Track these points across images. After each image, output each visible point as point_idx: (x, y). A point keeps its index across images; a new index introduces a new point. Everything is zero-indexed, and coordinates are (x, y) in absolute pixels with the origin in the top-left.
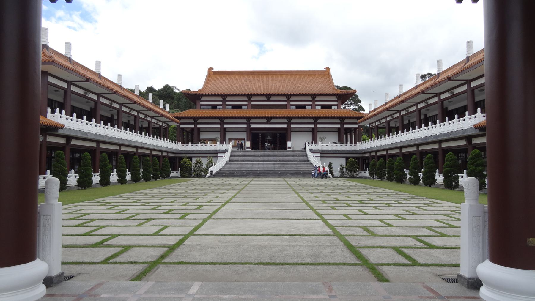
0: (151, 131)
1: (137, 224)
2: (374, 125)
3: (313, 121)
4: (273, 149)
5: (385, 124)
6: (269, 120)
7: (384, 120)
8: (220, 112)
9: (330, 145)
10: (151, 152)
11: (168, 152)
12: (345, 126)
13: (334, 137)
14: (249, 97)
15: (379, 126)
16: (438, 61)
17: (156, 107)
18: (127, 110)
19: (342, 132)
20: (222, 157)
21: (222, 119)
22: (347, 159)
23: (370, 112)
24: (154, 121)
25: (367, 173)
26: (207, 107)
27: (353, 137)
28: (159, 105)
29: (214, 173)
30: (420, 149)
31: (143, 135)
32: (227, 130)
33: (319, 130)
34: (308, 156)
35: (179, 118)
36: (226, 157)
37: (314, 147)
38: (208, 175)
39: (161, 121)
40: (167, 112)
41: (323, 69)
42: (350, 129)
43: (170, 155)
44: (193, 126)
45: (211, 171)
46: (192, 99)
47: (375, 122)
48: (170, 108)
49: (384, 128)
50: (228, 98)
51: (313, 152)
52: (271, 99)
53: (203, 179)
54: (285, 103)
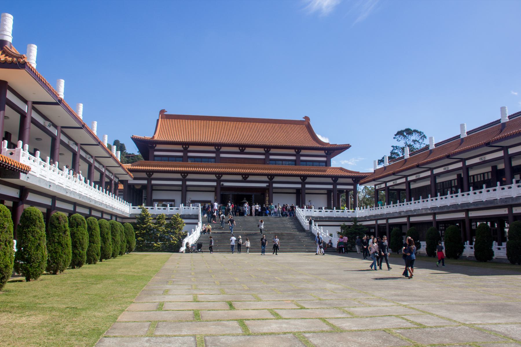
3: (146, 176)
6: (245, 177)
12: (339, 187)
13: (323, 200)
22: (343, 227)
30: (437, 218)
32: (154, 188)
33: (274, 190)
38: (183, 249)
41: (301, 118)
44: (145, 182)
45: (187, 244)
54: (263, 157)
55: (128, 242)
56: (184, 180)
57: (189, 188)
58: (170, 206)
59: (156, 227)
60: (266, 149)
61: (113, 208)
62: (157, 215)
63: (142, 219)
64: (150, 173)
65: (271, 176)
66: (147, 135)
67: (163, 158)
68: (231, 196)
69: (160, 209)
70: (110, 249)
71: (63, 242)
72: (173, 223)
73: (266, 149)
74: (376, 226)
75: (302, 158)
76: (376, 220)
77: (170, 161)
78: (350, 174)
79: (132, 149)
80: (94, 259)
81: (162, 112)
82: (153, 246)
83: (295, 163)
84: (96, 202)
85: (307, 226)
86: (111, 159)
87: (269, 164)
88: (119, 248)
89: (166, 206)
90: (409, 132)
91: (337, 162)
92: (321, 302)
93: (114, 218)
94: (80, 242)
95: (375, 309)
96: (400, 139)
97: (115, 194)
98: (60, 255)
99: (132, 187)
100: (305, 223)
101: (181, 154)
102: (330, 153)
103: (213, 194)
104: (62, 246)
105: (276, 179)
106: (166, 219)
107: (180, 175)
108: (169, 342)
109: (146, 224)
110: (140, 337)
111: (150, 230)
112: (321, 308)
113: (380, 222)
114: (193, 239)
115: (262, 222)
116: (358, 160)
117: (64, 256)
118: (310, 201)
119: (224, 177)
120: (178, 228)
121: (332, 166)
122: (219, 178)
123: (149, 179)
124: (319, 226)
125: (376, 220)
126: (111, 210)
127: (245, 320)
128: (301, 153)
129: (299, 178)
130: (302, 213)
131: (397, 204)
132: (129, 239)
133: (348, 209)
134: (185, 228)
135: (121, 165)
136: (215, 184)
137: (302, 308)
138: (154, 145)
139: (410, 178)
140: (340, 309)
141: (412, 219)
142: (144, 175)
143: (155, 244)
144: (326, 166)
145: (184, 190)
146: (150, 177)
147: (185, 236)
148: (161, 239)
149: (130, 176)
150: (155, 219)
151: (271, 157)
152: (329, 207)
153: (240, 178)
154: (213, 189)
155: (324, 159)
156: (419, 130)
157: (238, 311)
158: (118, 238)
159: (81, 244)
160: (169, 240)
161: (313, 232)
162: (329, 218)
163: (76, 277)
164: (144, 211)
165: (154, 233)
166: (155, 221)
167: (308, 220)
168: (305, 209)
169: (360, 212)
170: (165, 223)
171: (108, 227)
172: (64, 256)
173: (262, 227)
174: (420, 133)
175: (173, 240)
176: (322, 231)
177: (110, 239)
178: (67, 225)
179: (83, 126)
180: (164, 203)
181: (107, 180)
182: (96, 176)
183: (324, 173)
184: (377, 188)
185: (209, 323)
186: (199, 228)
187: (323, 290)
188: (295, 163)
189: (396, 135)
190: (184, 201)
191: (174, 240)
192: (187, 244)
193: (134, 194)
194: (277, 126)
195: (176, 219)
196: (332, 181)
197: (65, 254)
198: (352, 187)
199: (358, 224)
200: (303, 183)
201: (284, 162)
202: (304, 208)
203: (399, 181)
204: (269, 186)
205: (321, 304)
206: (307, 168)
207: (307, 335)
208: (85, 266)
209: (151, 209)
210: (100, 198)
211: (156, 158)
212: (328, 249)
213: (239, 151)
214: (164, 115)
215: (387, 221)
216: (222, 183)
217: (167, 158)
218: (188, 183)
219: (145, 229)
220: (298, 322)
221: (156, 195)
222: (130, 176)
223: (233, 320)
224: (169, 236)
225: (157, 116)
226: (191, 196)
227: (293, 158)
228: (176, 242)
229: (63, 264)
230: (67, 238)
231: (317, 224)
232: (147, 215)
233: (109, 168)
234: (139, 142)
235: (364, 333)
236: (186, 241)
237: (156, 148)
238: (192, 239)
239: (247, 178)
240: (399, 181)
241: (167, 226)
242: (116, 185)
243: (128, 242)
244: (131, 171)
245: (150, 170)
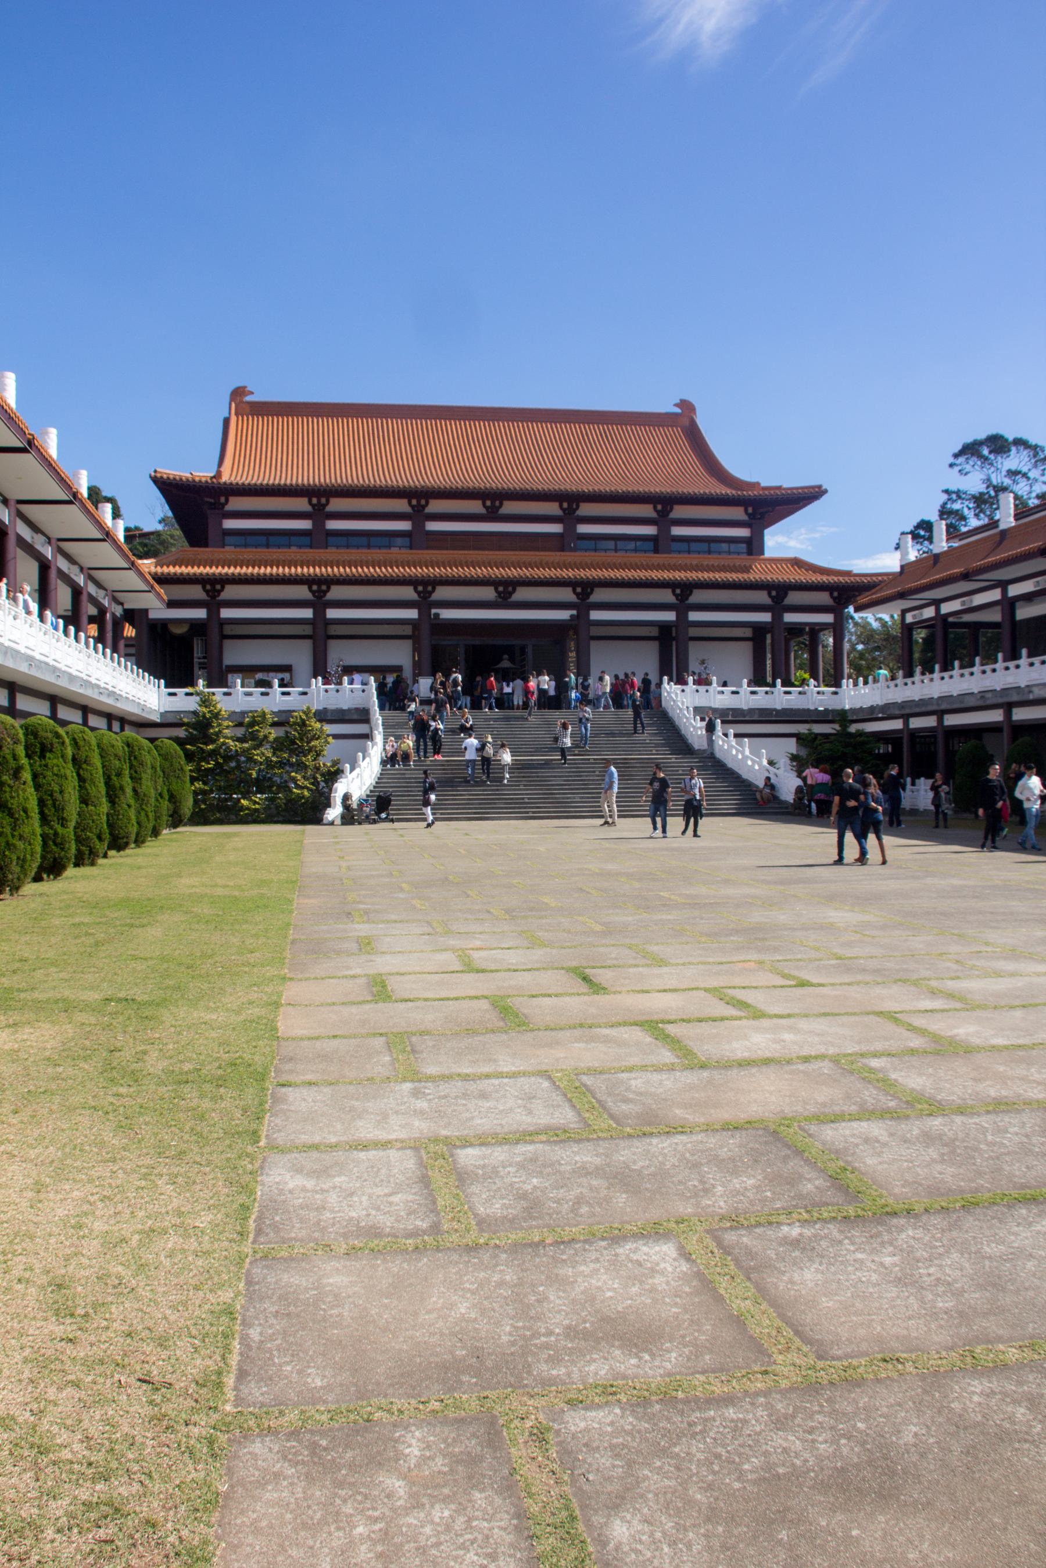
6: (505, 592)
12: (790, 618)
13: (741, 656)
26: (733, 547)
32: (228, 630)
33: (594, 631)
38: (334, 813)
41: (668, 406)
44: (201, 614)
45: (346, 797)
50: (586, 509)
54: (556, 528)
55: (172, 798)
56: (319, 604)
57: (334, 630)
58: (280, 686)
59: (245, 751)
60: (659, 507)
61: (117, 697)
62: (243, 713)
63: (200, 728)
64: (213, 585)
65: (585, 588)
66: (199, 469)
67: (354, 540)
68: (461, 650)
70: (129, 819)
71: (14, 804)
72: (295, 737)
73: (488, 503)
74: (905, 733)
75: (677, 531)
76: (906, 717)
77: (375, 547)
78: (825, 578)
79: (151, 513)
80: (91, 852)
81: (238, 393)
82: (237, 807)
83: (656, 544)
84: (72, 678)
85: (700, 737)
86: (106, 546)
87: (575, 550)
88: (151, 815)
89: (268, 684)
90: (998, 444)
91: (783, 541)
92: (845, 965)
93: (116, 726)
94: (54, 801)
95: (1019, 982)
96: (968, 468)
97: (115, 650)
98: (7, 843)
99: (159, 630)
100: (694, 729)
101: (305, 525)
102: (762, 515)
103: (408, 645)
104: (11, 814)
105: (599, 595)
106: (274, 724)
107: (669, 591)
108: (484, 1096)
109: (213, 741)
110: (382, 1082)
111: (228, 758)
112: (858, 983)
113: (915, 723)
114: (362, 783)
115: (565, 726)
116: (817, 535)
117: (20, 845)
118: (703, 662)
119: (442, 593)
120: (310, 750)
121: (768, 554)
122: (319, 595)
123: (213, 604)
124: (736, 736)
125: (906, 717)
126: (110, 701)
127: (663, 1022)
128: (428, 510)
129: (570, 589)
130: (681, 699)
131: (975, 669)
132: (174, 787)
133: (819, 686)
134: (331, 752)
135: (133, 563)
136: (412, 614)
137: (803, 984)
138: (223, 500)
139: (1014, 590)
140: (916, 983)
141: (1020, 715)
142: (197, 592)
143: (244, 802)
144: (750, 553)
145: (320, 636)
146: (213, 597)
147: (333, 775)
148: (262, 784)
149: (158, 595)
150: (240, 724)
151: (583, 529)
152: (758, 679)
153: (488, 593)
154: (408, 630)
155: (743, 532)
156: (1033, 441)
157: (619, 997)
158: (147, 786)
159: (59, 809)
160: (284, 787)
161: (718, 754)
162: (762, 711)
163: (68, 907)
164: (205, 702)
165: (238, 767)
166: (240, 732)
167: (702, 719)
168: (691, 686)
169: (854, 695)
170: (272, 737)
171: (121, 753)
172: (20, 845)
173: (568, 742)
174: (1035, 449)
175: (298, 787)
176: (747, 752)
177: (129, 791)
178: (21, 751)
179: (30, 443)
180: (259, 676)
181: (93, 611)
182: (63, 596)
183: (746, 576)
184: (909, 618)
185: (560, 1034)
186: (376, 750)
187: (829, 928)
188: (656, 544)
189: (956, 456)
190: (320, 669)
191: (301, 787)
192: (346, 797)
193: (167, 653)
194: (594, 431)
195: (303, 724)
196: (309, 596)
197: (21, 837)
198: (828, 618)
199: (853, 728)
200: (682, 607)
201: (620, 544)
202: (685, 683)
203: (979, 599)
204: (578, 616)
205: (849, 970)
206: (694, 559)
207: (875, 1063)
208: (71, 871)
209: (263, 694)
210: (80, 666)
211: (228, 539)
212: (758, 802)
213: (483, 511)
214: (246, 406)
215: (940, 720)
216: (433, 611)
217: (263, 539)
218: (332, 613)
219: (214, 753)
220: (820, 1025)
221: (235, 654)
222: (158, 595)
223: (625, 1024)
224: (286, 777)
225: (222, 407)
226: (339, 653)
227: (650, 530)
228: (306, 793)
229: (17, 869)
230: (24, 791)
231: (731, 732)
232: (216, 715)
233: (99, 575)
234: (178, 493)
235: (1034, 1053)
236: (340, 788)
237: (229, 507)
238: (357, 782)
239: (511, 594)
240: (979, 599)
241: (279, 745)
242: (118, 625)
243: (172, 798)
244: (162, 580)
245: (211, 575)
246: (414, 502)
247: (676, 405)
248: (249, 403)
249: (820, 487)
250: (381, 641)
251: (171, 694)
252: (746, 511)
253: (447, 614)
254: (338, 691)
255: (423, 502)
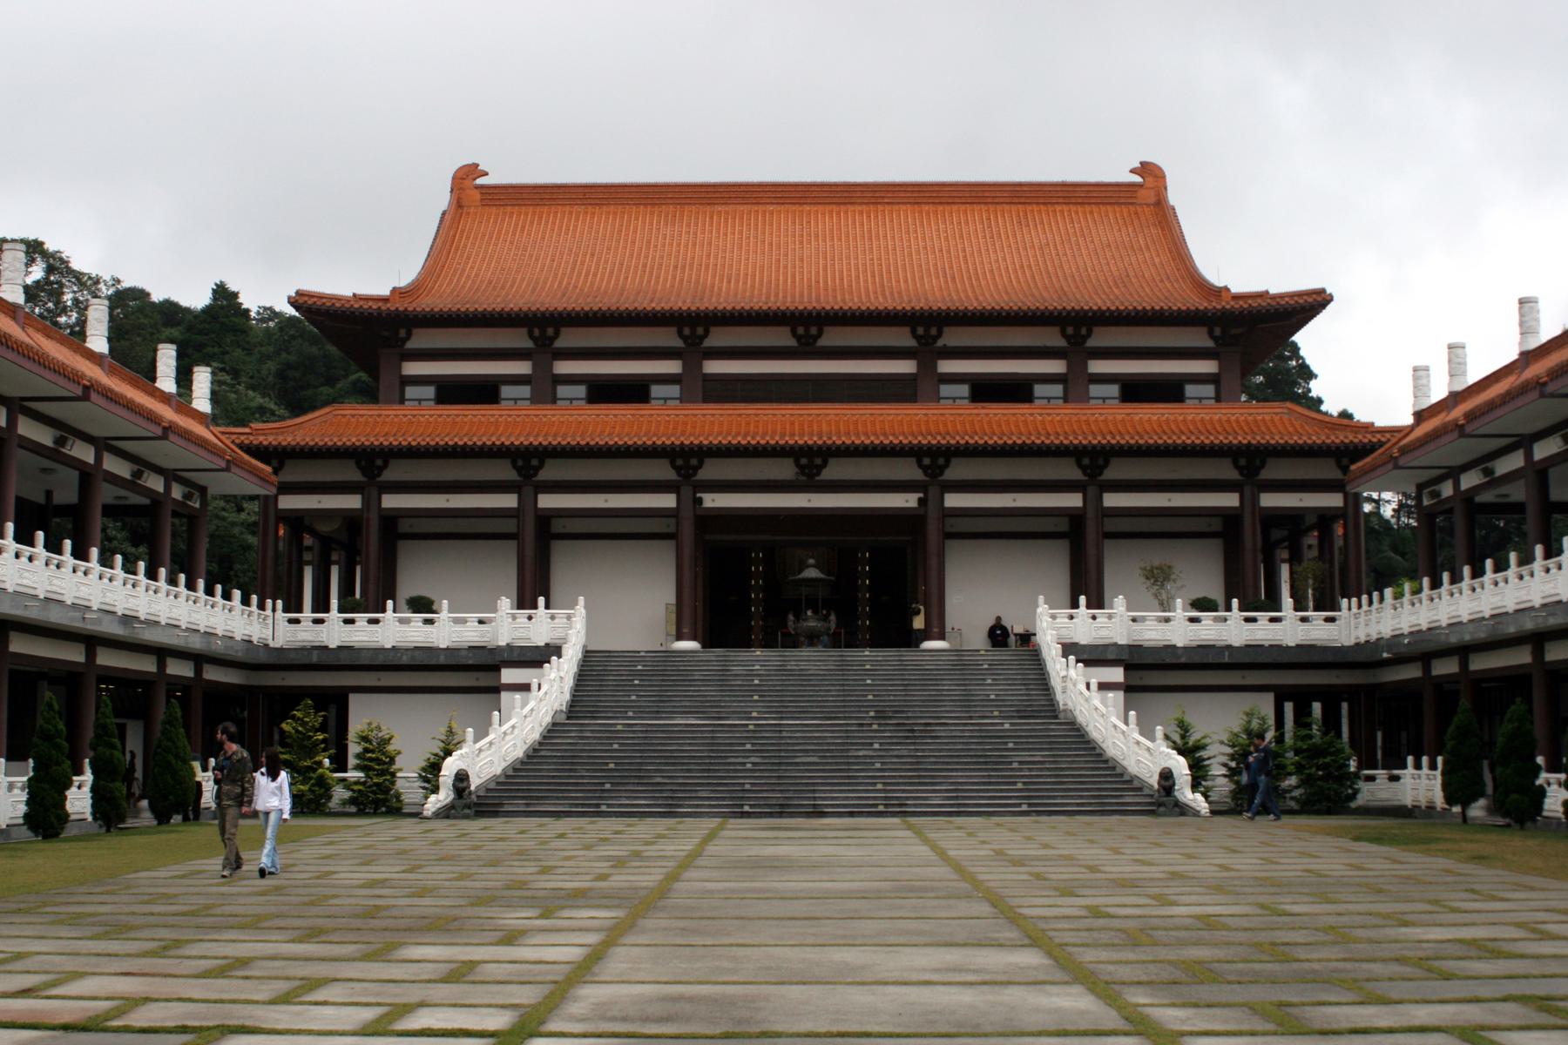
0: (202, 564)
1: (272, 995)
2: (1447, 490)
3: (916, 474)
4: (835, 643)
5: (1517, 492)
6: (810, 464)
7: (1515, 461)
8: (514, 421)
9: (1180, 612)
10: (91, 655)
11: (199, 659)
12: (1269, 500)
14: (693, 329)
15: (1486, 497)
16: (1522, 302)
17: (135, 384)
18: (44, 436)
19: (1251, 537)
20: (525, 688)
21: (527, 464)
23: (1420, 416)
24: (112, 465)
25: (1420, 784)
27: (1285, 571)
28: (151, 375)
29: (475, 783)
31: (162, 583)
33: (1112, 525)
34: (1056, 682)
35: (276, 456)
36: (553, 688)
37: (1086, 626)
39: (158, 470)
40: (164, 398)
41: (1122, 174)
42: (1292, 520)
43: (212, 674)
44: (353, 502)
45: (461, 778)
46: (349, 342)
47: (1454, 473)
48: (215, 397)
49: (1519, 508)
51: (1091, 656)
52: (824, 342)
53: (406, 827)
54: (905, 367)
69: (1144, 619)
73: (920, 331)
107: (665, 463)
129: (913, 461)
136: (668, 501)
138: (403, 333)
192: (461, 778)
198: (1334, 500)
231: (1094, 683)
239: (696, 469)
246: (801, 330)
247: (1132, 171)
248: (482, 187)
249: (1323, 291)
250: (1123, 541)
251: (1247, 620)
252: (914, 333)
253: (713, 501)
254: (530, 618)
255: (814, 331)
